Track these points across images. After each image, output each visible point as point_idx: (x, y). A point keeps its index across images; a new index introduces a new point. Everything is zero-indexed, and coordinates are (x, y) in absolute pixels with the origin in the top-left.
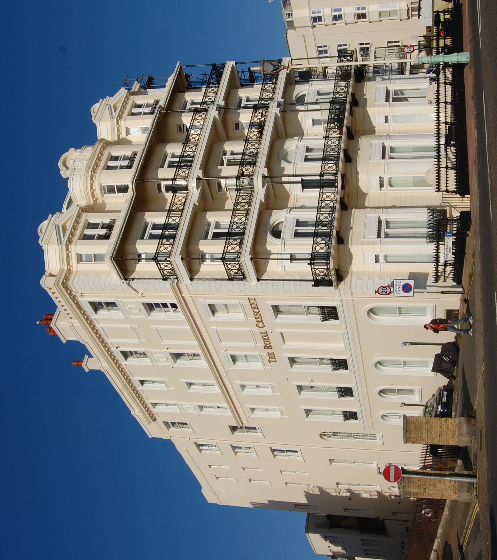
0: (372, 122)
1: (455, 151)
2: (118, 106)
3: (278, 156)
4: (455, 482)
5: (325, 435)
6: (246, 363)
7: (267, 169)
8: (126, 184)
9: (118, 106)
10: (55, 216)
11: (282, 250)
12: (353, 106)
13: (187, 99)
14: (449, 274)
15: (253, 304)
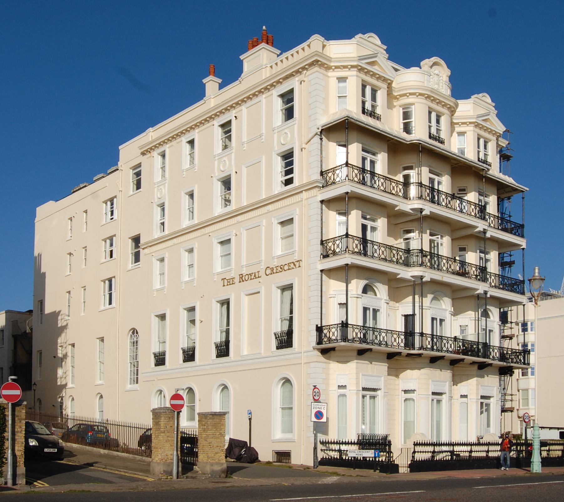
0: (462, 383)
1: (445, 459)
2: (488, 123)
3: (439, 291)
4: (172, 459)
5: (133, 333)
6: (219, 255)
7: (429, 280)
8: (414, 132)
9: (487, 123)
10: (385, 52)
11: (352, 295)
12: (479, 365)
13: (490, 197)
14: (327, 454)
15: (295, 264)
